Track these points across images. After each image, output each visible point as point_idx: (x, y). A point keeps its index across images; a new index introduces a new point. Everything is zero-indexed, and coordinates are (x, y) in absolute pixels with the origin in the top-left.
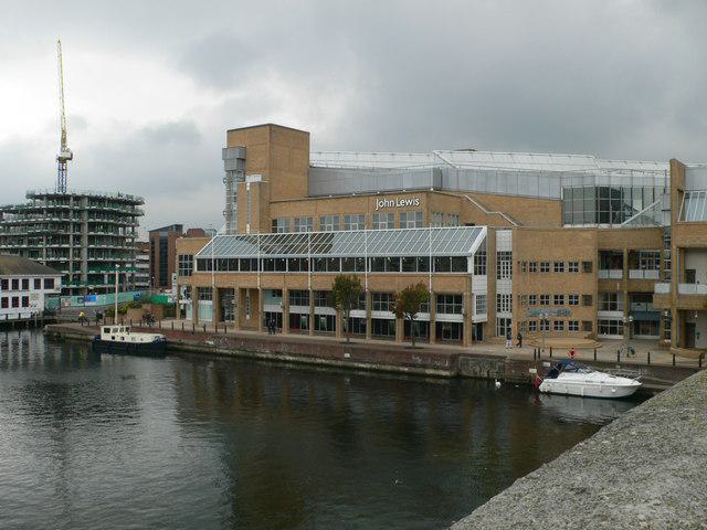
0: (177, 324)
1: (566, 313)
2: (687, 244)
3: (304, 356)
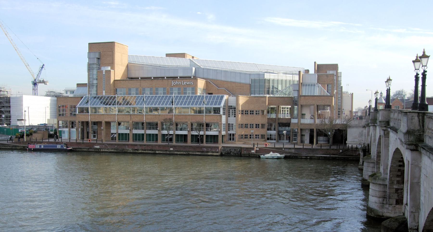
0: (187, 228)
3: (150, 150)
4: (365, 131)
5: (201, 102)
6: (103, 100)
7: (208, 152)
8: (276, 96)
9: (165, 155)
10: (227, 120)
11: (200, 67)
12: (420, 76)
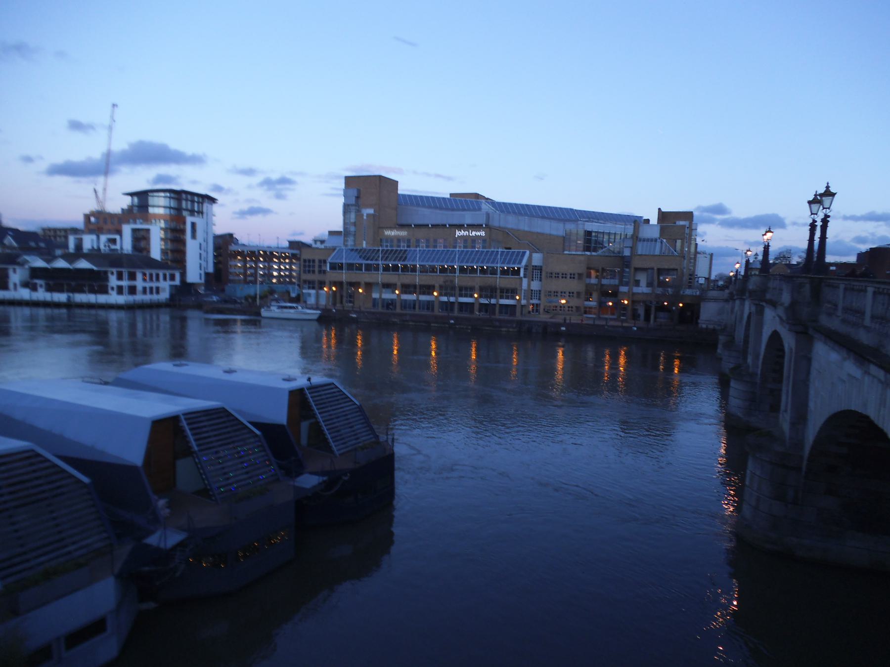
4: (728, 306)
5: (494, 259)
6: (363, 253)
10: (529, 285)
12: (819, 224)
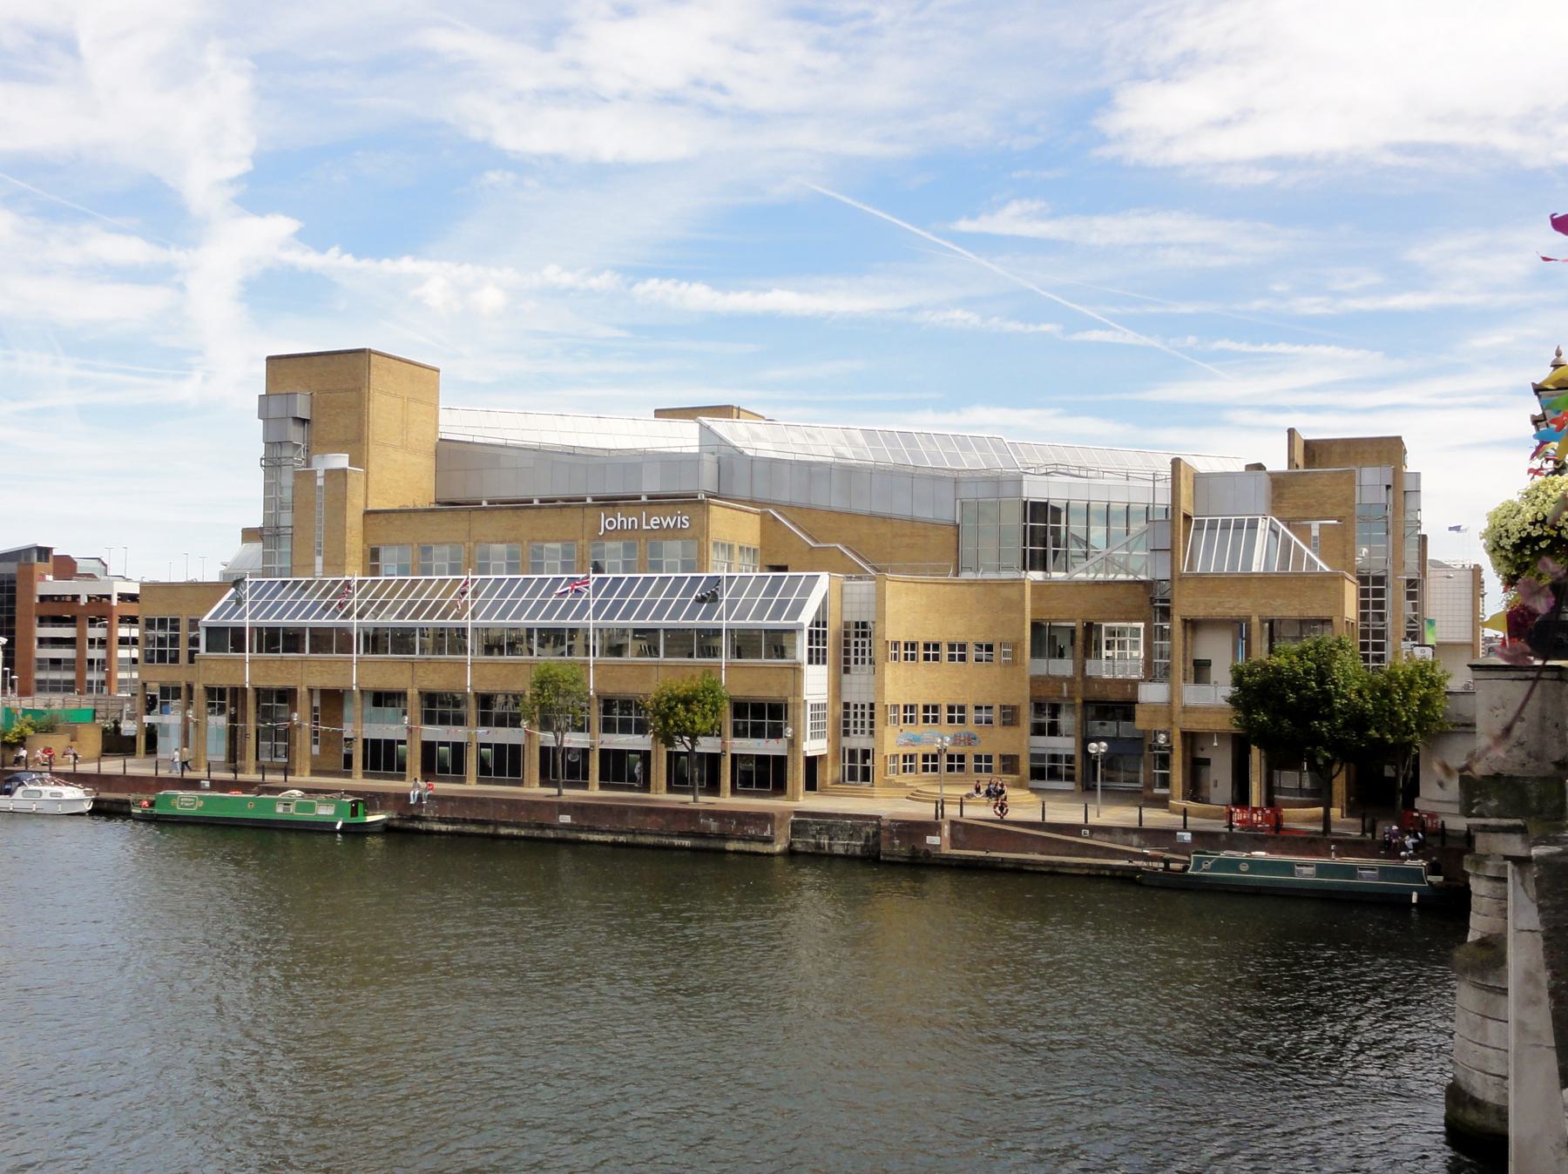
1: (970, 740)
2: (1199, 612)
3: (474, 822)
7: (724, 837)
8: (1081, 576)
9: (189, 829)
10: (837, 688)
11: (742, 453)
